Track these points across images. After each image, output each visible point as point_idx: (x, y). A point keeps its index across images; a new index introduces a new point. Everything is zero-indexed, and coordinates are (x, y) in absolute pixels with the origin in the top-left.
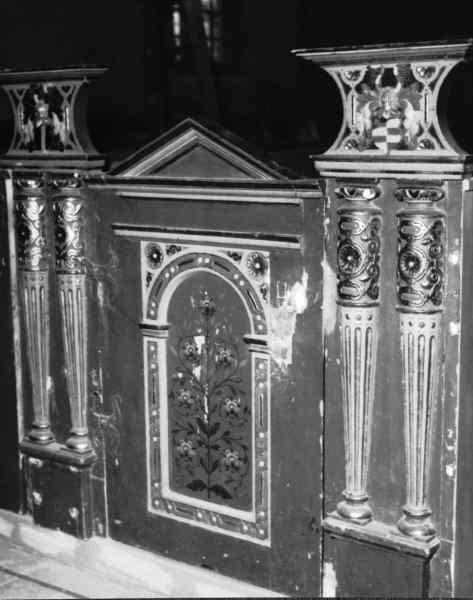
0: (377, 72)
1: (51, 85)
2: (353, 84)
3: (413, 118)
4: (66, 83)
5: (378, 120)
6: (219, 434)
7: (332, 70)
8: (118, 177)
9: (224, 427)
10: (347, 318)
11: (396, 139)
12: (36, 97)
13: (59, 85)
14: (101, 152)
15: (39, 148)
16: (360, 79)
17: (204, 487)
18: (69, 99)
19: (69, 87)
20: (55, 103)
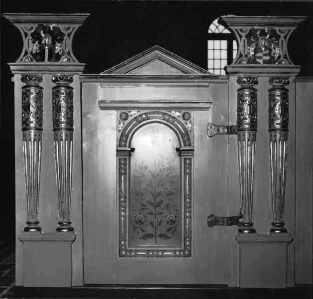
0: (257, 30)
1: (53, 25)
2: (29, 33)
3: (277, 52)
4: (282, 28)
5: (256, 51)
6: (163, 206)
7: (17, 25)
8: (133, 73)
9: (166, 202)
10: (170, 140)
11: (268, 58)
12: (42, 32)
13: (61, 27)
14: (295, 64)
15: (43, 59)
16: (33, 31)
17: (153, 236)
18: (69, 35)
19: (70, 28)
20: (57, 37)
